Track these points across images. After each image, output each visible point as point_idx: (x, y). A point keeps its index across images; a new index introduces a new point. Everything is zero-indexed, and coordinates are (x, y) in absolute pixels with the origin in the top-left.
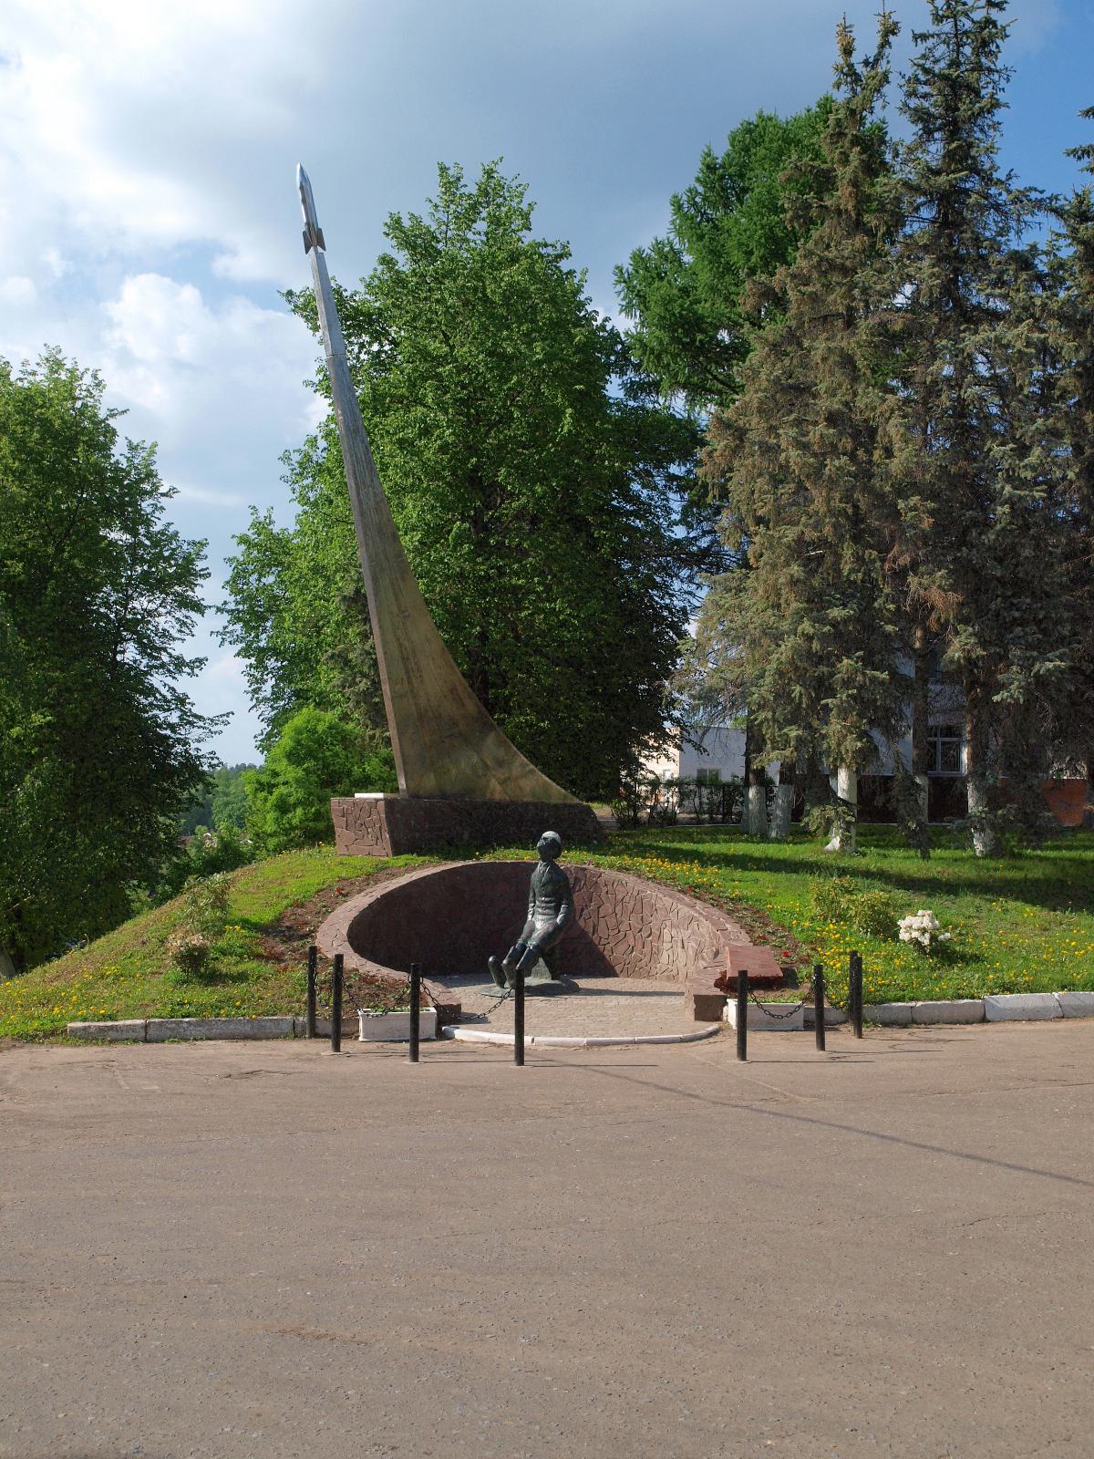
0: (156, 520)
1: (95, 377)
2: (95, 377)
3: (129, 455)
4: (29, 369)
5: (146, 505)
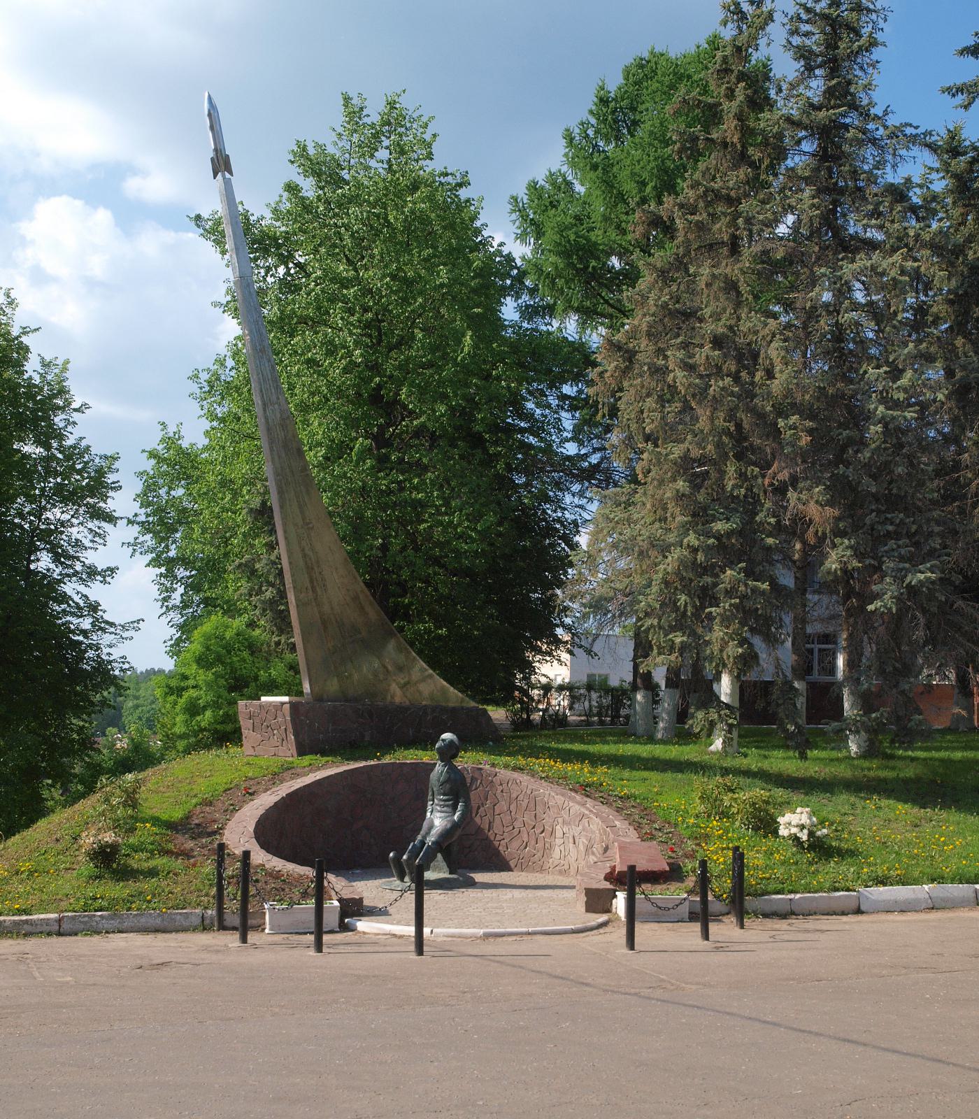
5: (59, 420)
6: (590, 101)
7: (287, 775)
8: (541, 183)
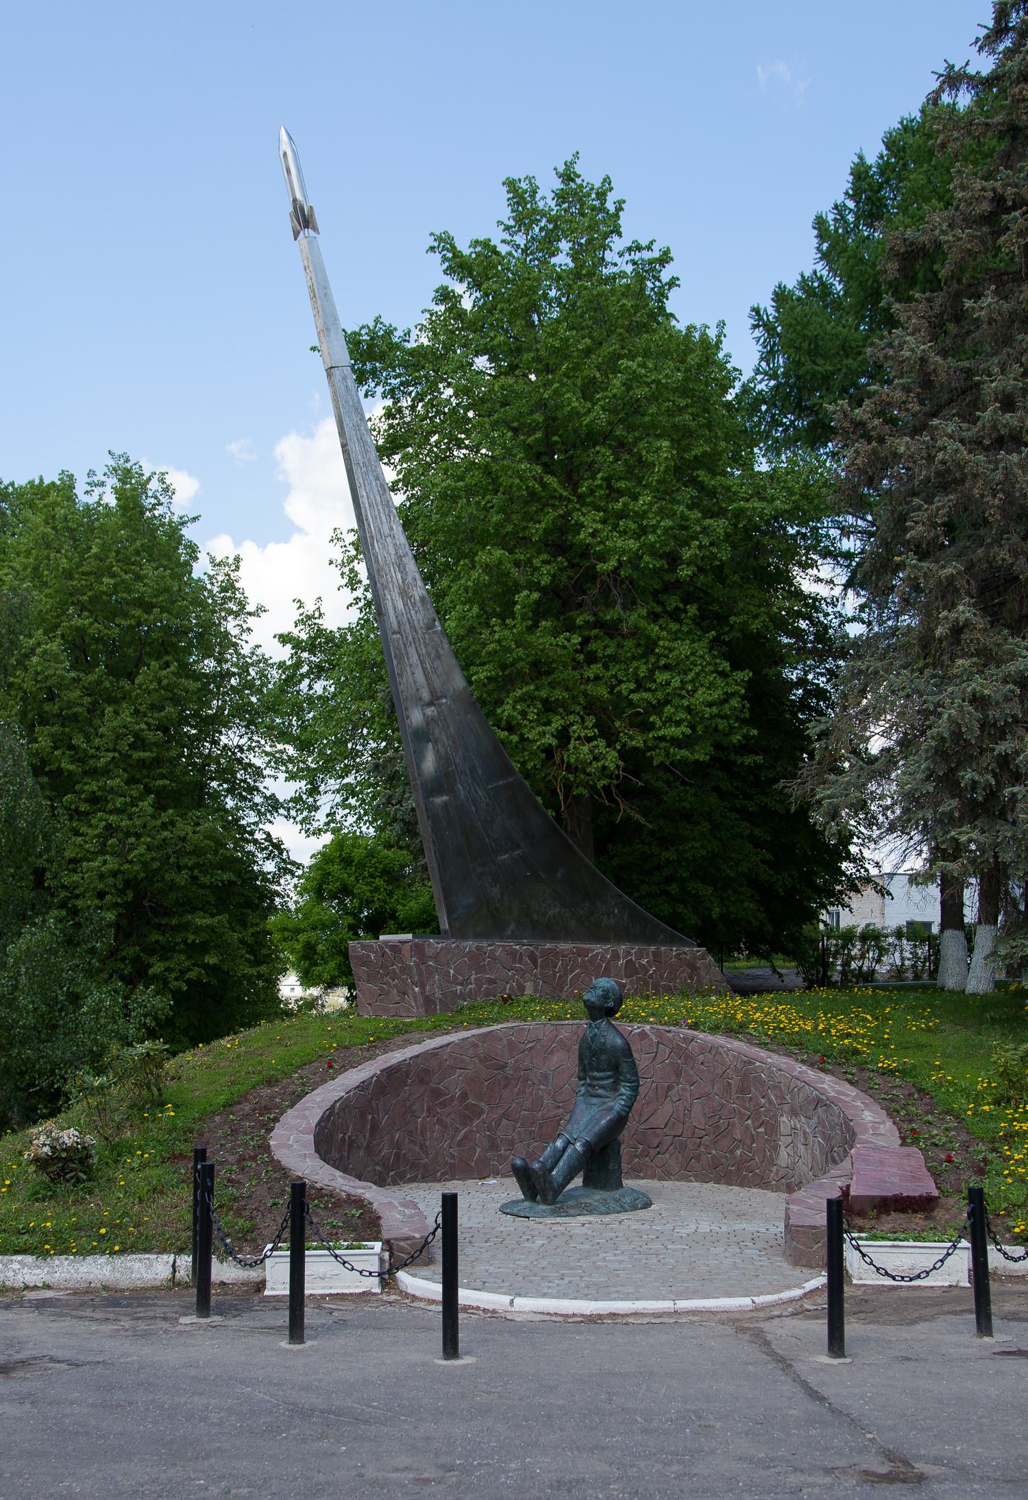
0: (243, 643)
1: (162, 481)
2: (162, 481)
3: (212, 573)
4: (95, 479)
5: (231, 625)
6: (844, 182)
7: (398, 1039)
8: (790, 286)
